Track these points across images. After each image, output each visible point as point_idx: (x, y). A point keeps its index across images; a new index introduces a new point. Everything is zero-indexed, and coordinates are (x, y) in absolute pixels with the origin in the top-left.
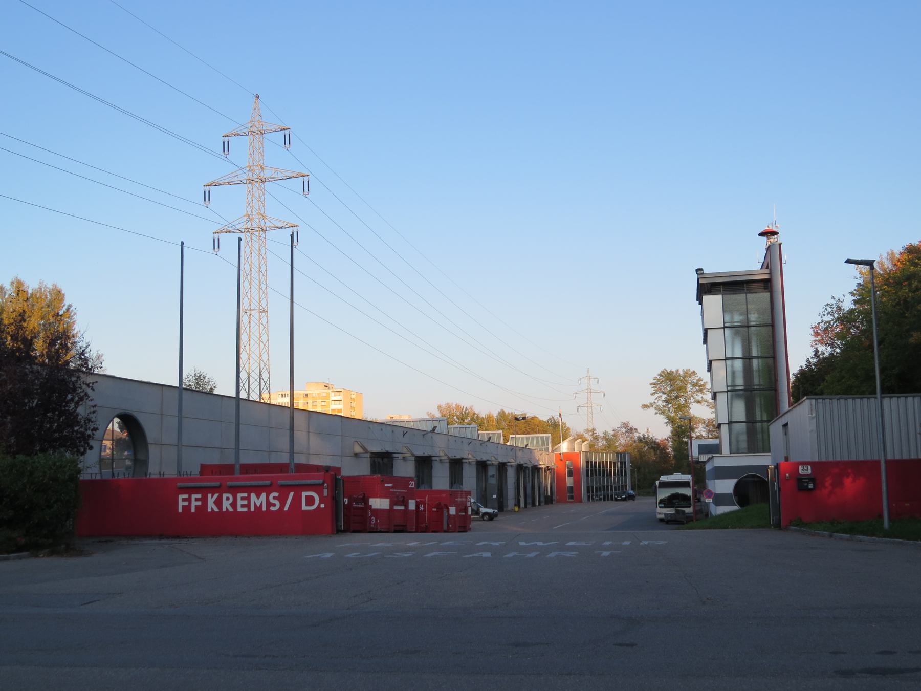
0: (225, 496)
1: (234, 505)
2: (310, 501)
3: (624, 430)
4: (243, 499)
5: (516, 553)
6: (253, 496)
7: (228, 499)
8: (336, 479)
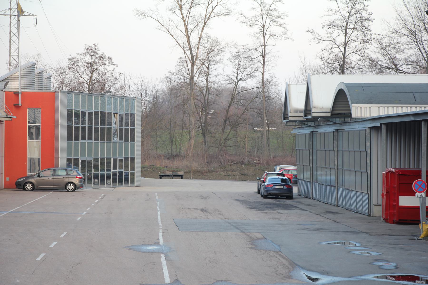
3: (88, 59)
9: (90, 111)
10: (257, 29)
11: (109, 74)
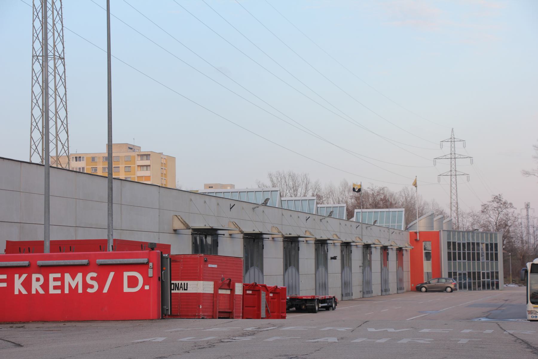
0: (34, 276)
1: (45, 286)
2: (133, 282)
3: (495, 205)
4: (55, 279)
5: (364, 339)
6: (67, 276)
7: (38, 280)
8: (162, 257)
9: (464, 242)
11: (510, 215)
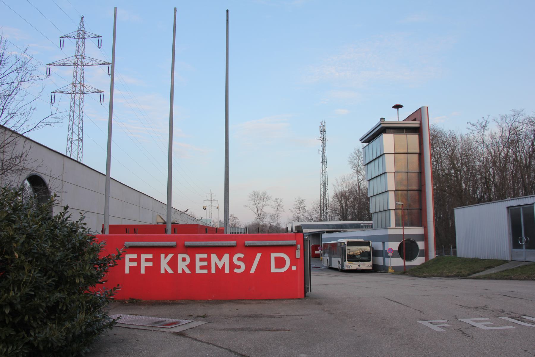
10: (276, 209)
